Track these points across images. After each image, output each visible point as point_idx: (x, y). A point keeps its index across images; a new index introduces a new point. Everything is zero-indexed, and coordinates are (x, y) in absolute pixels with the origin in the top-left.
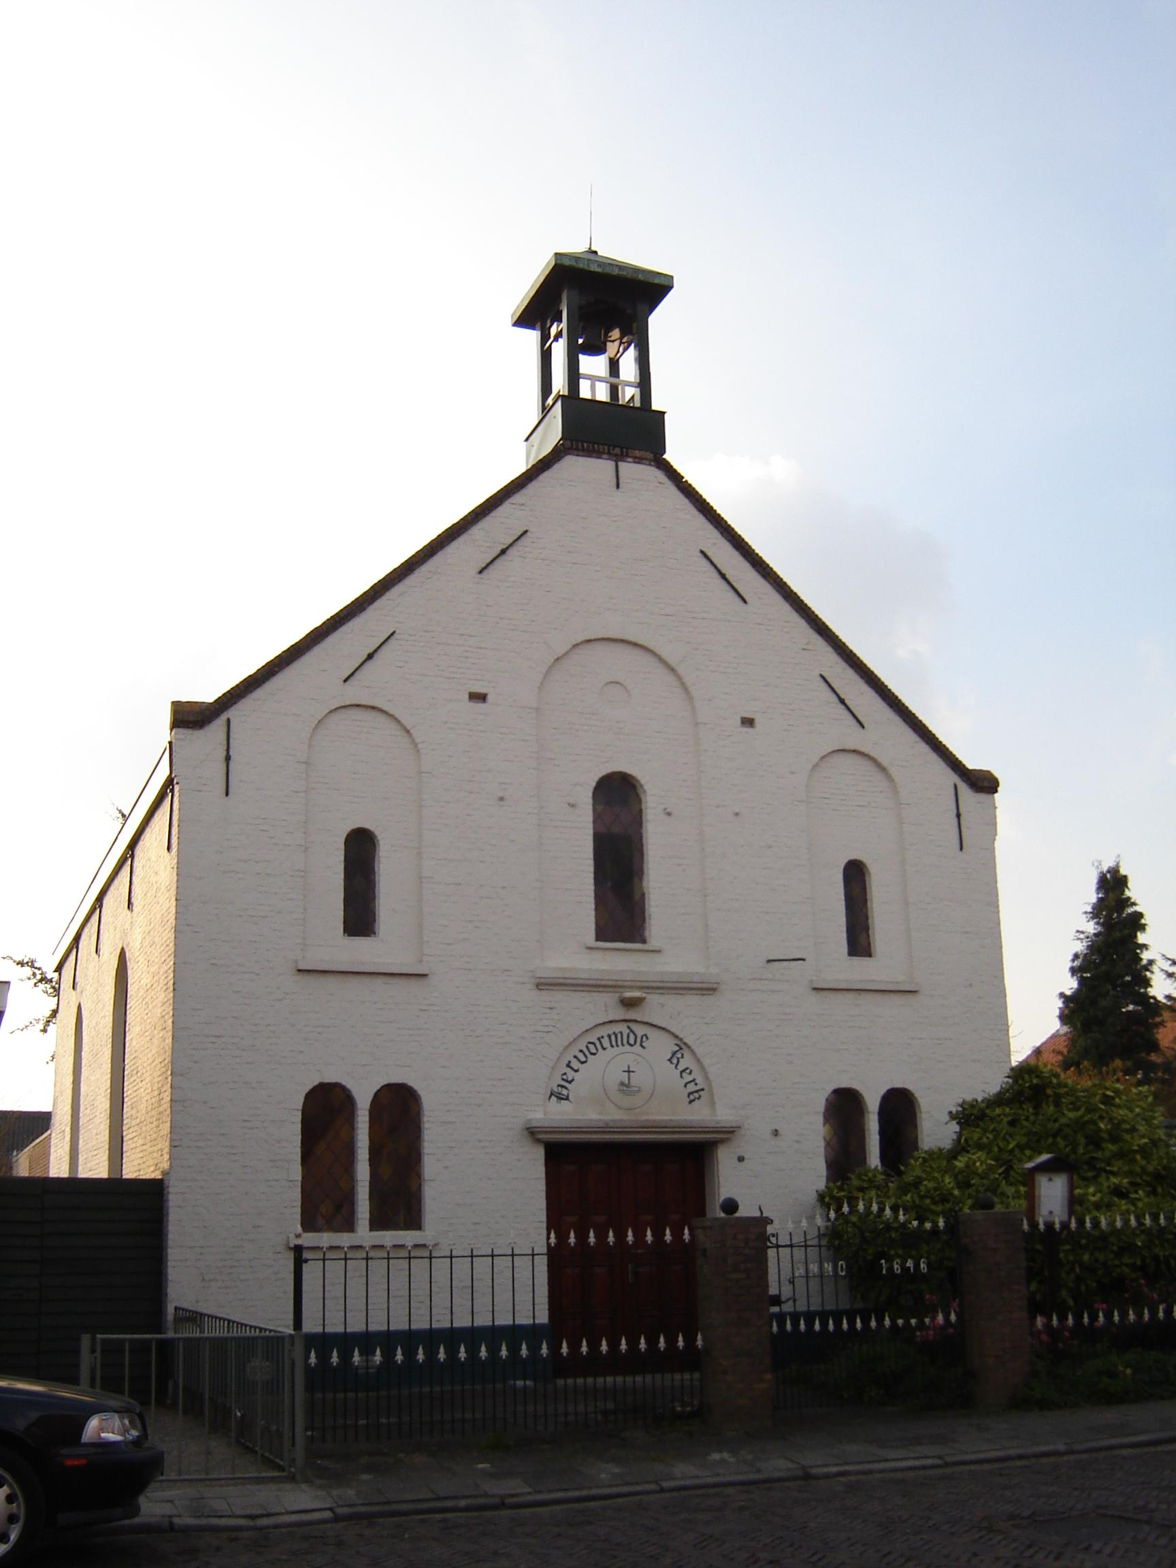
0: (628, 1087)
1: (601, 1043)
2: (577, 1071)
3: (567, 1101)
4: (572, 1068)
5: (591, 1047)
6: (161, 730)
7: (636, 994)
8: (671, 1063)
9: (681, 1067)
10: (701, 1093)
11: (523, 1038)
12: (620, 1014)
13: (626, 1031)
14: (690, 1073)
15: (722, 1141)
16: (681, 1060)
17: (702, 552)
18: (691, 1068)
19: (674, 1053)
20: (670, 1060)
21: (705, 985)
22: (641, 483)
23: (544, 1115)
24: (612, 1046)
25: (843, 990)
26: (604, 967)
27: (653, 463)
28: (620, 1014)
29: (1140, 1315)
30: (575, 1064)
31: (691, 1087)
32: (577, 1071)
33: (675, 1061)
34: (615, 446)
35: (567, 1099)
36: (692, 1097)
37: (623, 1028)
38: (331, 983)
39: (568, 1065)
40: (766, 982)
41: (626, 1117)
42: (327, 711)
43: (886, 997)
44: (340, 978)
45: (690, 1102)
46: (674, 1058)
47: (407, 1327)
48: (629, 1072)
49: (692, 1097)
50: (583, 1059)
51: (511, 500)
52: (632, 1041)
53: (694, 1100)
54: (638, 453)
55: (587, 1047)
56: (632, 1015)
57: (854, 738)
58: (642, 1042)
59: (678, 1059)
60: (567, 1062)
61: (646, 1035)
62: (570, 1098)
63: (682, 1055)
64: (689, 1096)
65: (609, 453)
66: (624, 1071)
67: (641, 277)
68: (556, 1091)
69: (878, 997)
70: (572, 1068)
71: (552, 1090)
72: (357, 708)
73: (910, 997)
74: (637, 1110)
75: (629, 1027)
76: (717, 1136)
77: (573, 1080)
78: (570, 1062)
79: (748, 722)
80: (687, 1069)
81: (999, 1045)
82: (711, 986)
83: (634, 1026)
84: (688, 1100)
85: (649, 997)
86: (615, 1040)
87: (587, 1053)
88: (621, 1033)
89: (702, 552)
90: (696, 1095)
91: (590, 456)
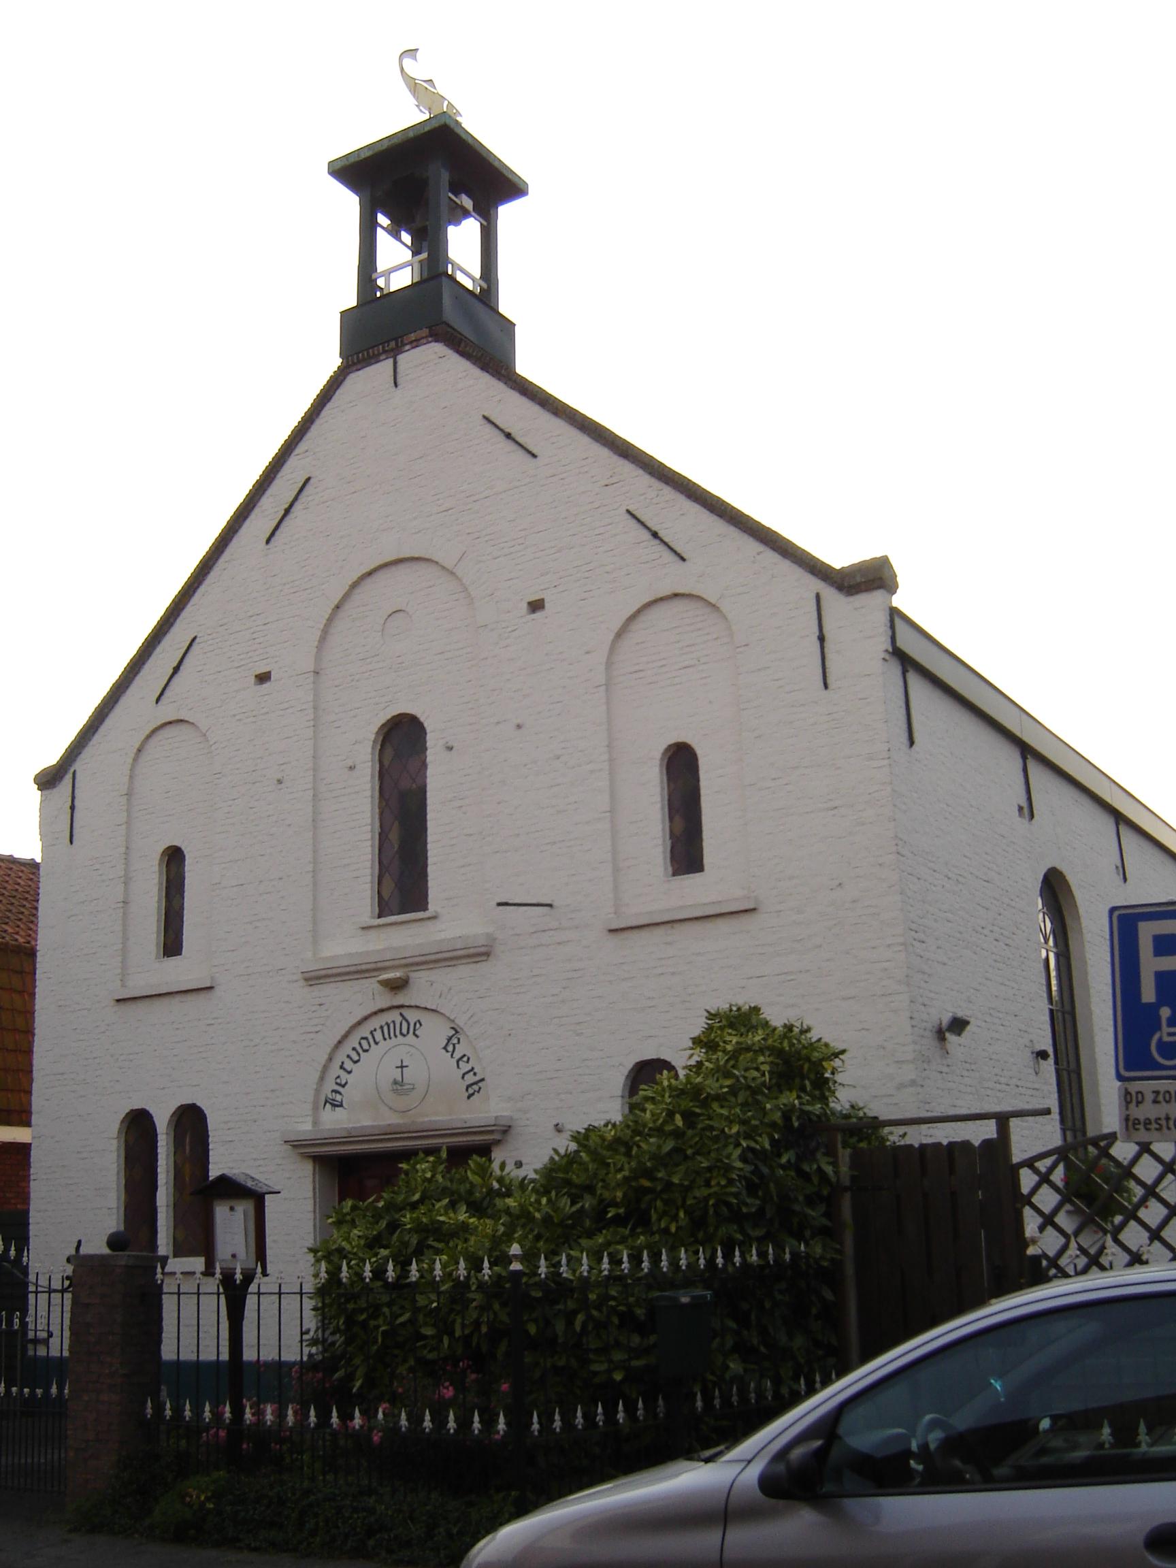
0: (401, 1086)
1: (374, 1038)
2: (350, 1072)
3: (341, 1108)
4: (344, 1069)
5: (364, 1043)
6: (35, 795)
7: (397, 974)
8: (447, 1051)
9: (457, 1055)
10: (480, 1084)
11: (294, 1042)
12: (385, 1000)
13: (398, 1019)
14: (468, 1061)
15: (498, 1142)
16: (457, 1046)
17: (485, 418)
18: (468, 1054)
19: (450, 1039)
20: (445, 1048)
21: (472, 951)
22: (421, 367)
23: (313, 1126)
24: (385, 1039)
25: (713, 916)
26: (371, 947)
27: (430, 339)
28: (385, 1000)
29: (281, 1415)
30: (349, 1065)
31: (470, 1078)
32: (350, 1072)
33: (450, 1048)
34: (388, 342)
35: (341, 1105)
36: (471, 1091)
37: (394, 1016)
38: (142, 1006)
39: (342, 1067)
40: (552, 932)
41: (401, 1121)
42: (611, 636)
43: (709, 926)
44: (147, 1002)
45: (469, 1097)
46: (450, 1044)
47: (175, 1358)
48: (402, 1067)
49: (471, 1091)
50: (356, 1058)
51: (297, 451)
52: (404, 1031)
53: (473, 1094)
54: (413, 336)
55: (360, 1044)
56: (400, 999)
57: (672, 578)
58: (415, 1030)
59: (454, 1045)
60: (340, 1064)
61: (419, 1021)
62: (344, 1105)
63: (459, 1040)
64: (467, 1090)
65: (385, 352)
66: (397, 1067)
67: (411, 134)
68: (331, 1097)
69: (698, 927)
70: (344, 1069)
71: (326, 1097)
72: (170, 725)
73: (745, 919)
74: (410, 1112)
75: (401, 1014)
76: (486, 1137)
77: (346, 1083)
78: (343, 1063)
79: (536, 606)
80: (464, 1055)
81: (886, 970)
82: (483, 950)
83: (406, 1012)
84: (467, 1094)
85: (412, 975)
86: (389, 1031)
87: (360, 1051)
88: (394, 1022)
89: (485, 418)
90: (476, 1087)
91: (370, 364)
